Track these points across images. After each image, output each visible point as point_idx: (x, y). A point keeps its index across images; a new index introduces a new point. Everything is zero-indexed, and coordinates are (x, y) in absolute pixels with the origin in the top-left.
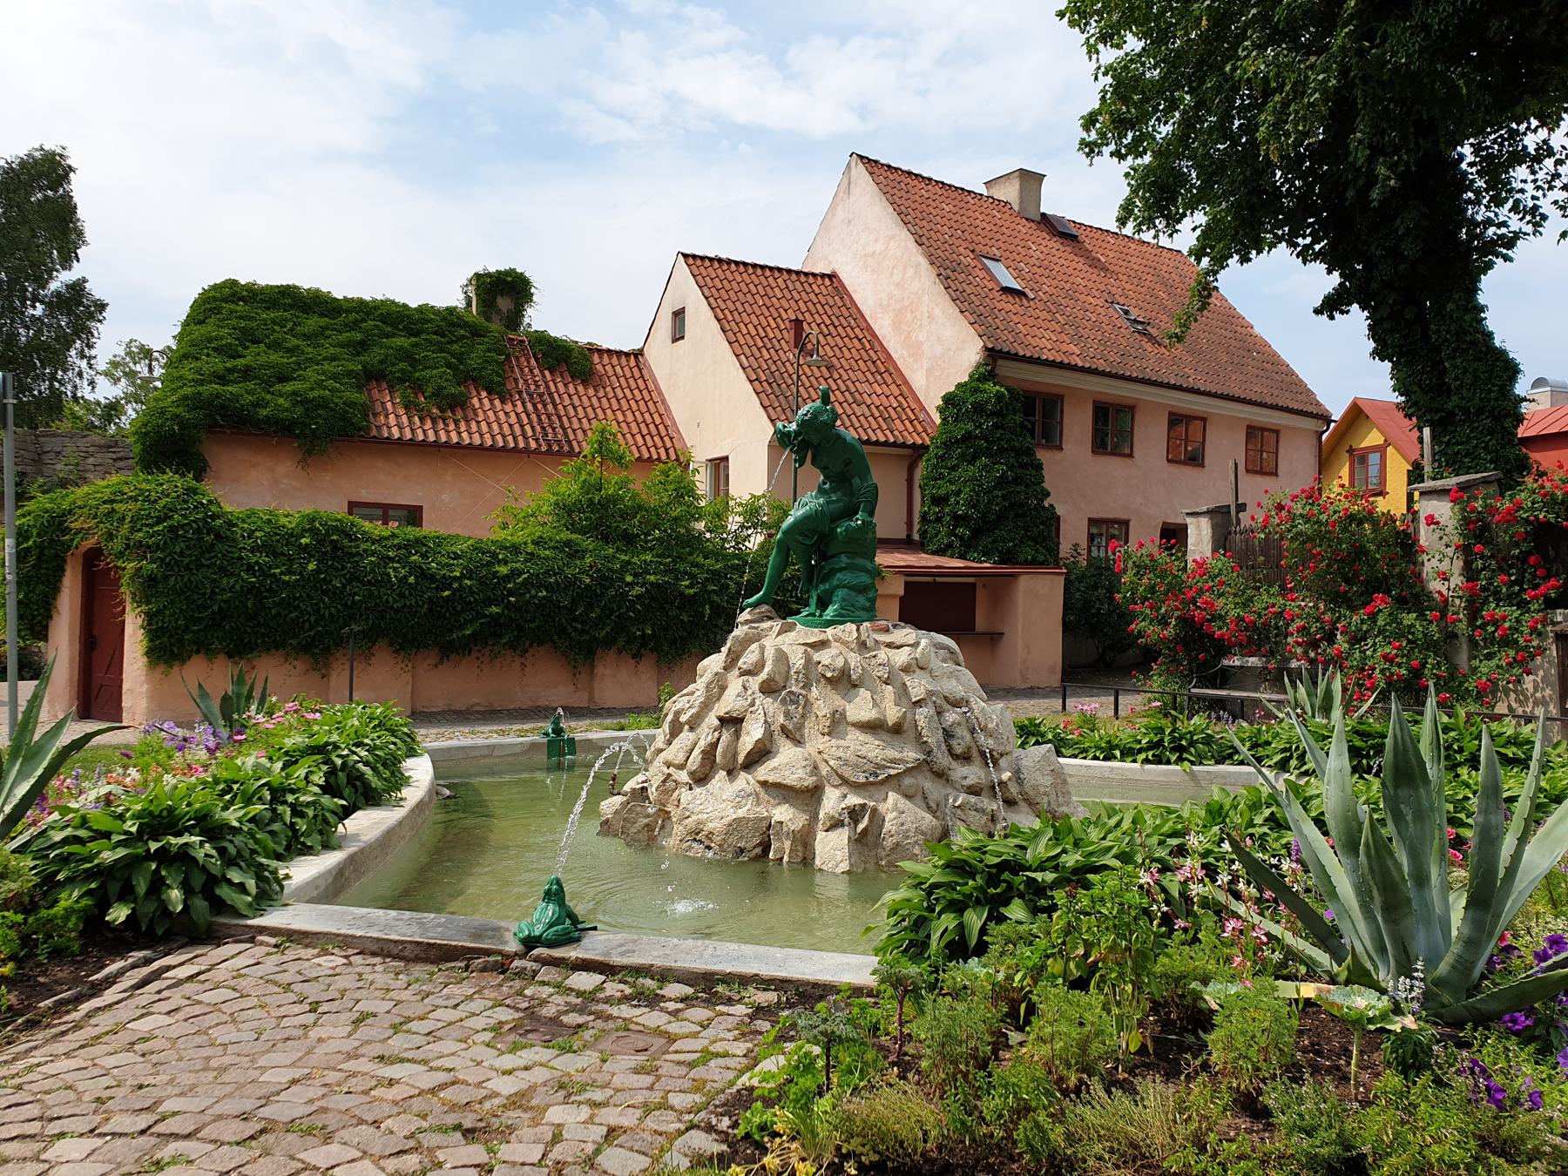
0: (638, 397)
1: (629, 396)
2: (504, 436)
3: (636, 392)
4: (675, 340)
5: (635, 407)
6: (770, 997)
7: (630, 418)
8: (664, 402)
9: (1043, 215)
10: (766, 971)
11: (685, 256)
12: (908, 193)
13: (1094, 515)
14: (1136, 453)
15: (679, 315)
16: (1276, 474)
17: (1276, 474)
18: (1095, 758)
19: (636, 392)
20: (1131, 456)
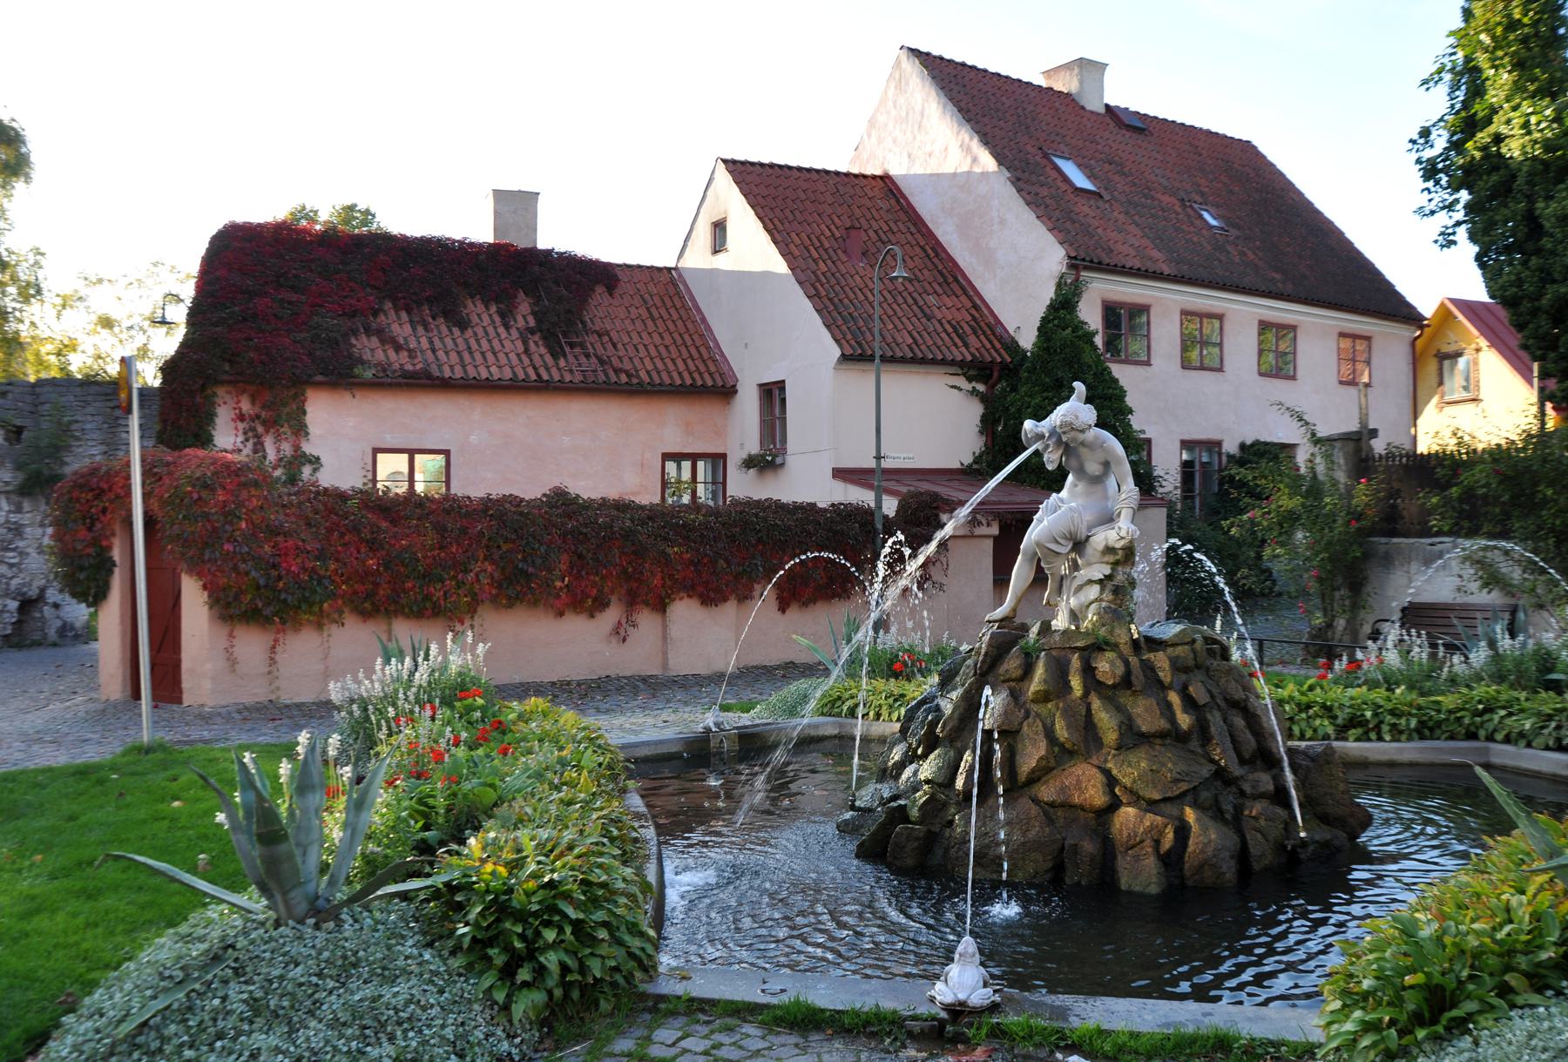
0: (675, 316)
1: (665, 316)
2: (547, 369)
3: (672, 311)
4: (715, 252)
5: (672, 328)
6: (1545, 877)
7: (668, 340)
8: (704, 320)
9: (1107, 106)
10: (1175, 1004)
11: (725, 161)
12: (970, 91)
13: (1187, 437)
14: (1300, 373)
15: (719, 227)
16: (1220, 370)
17: (1220, 370)
18: (1452, 738)
19: (672, 311)
20: (1293, 378)
